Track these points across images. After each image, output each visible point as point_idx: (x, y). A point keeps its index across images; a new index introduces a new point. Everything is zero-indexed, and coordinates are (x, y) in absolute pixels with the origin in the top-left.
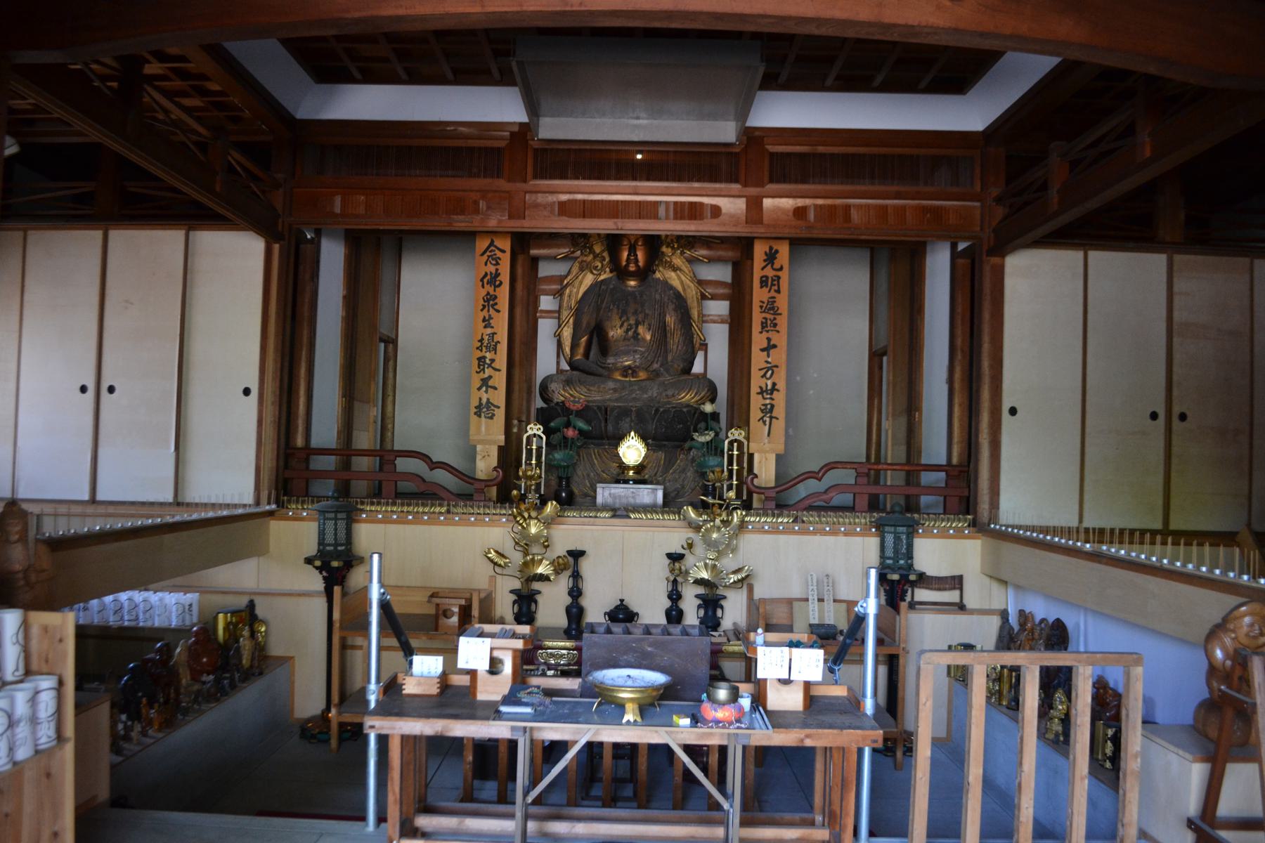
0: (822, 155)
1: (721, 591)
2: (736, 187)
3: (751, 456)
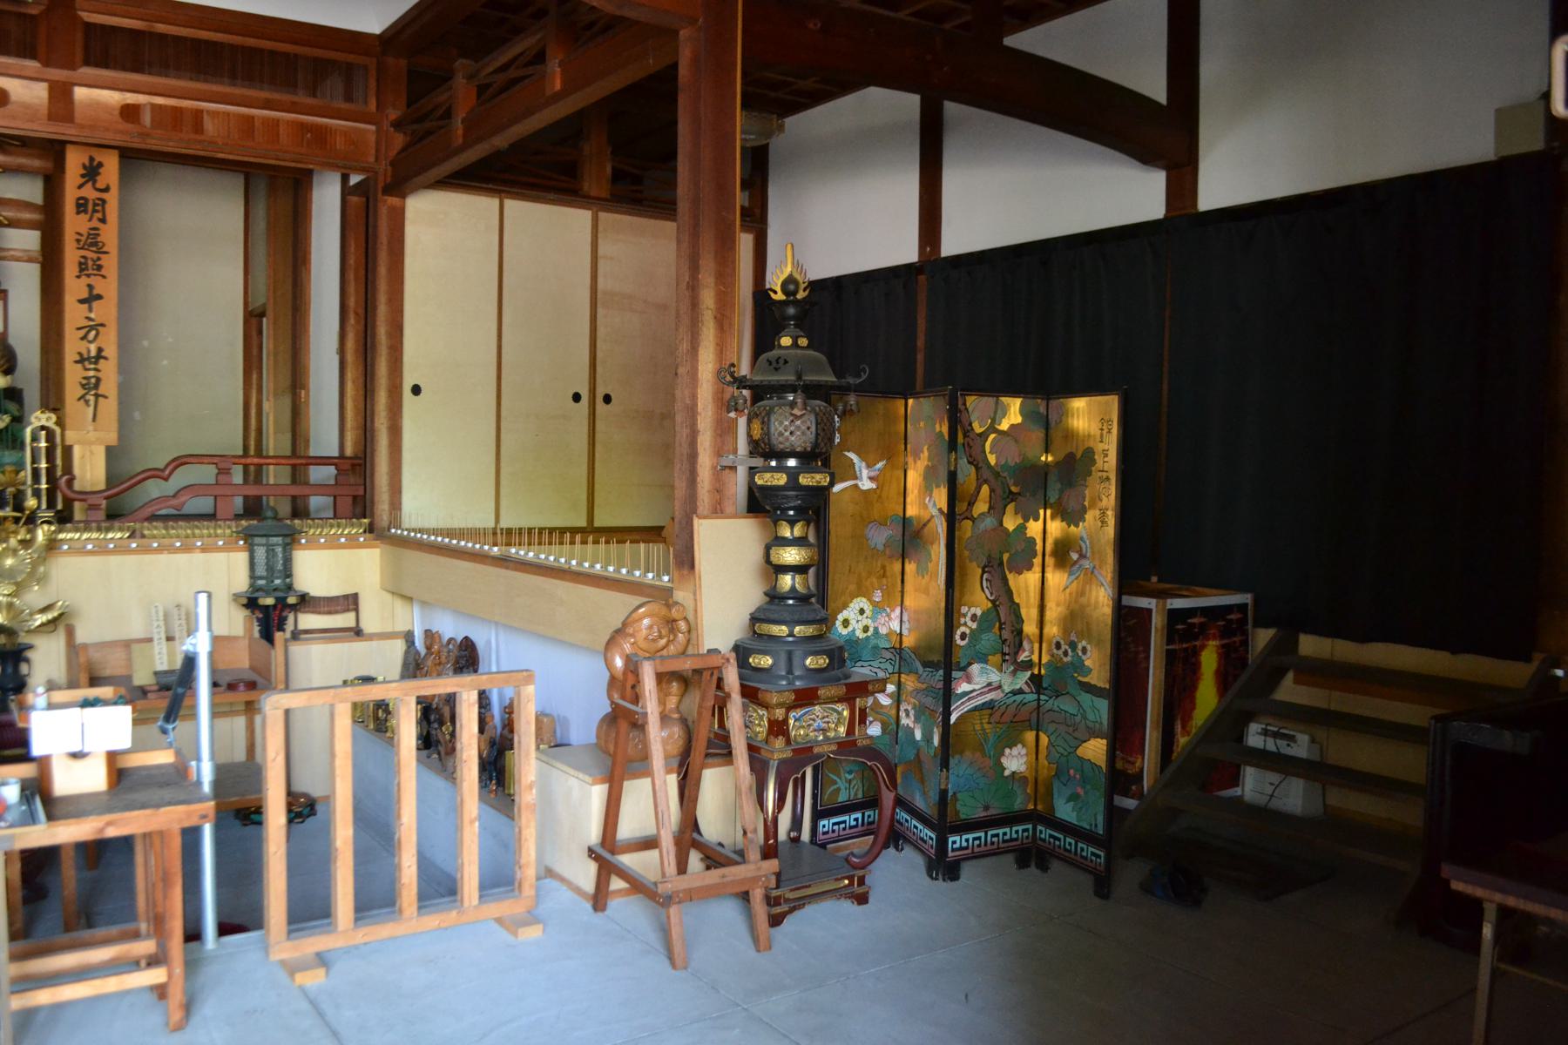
0: (163, 37)
1: (24, 639)
2: (32, 65)
3: (68, 451)
